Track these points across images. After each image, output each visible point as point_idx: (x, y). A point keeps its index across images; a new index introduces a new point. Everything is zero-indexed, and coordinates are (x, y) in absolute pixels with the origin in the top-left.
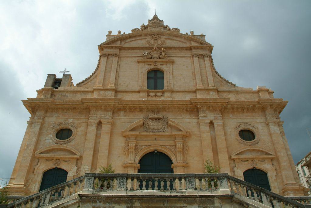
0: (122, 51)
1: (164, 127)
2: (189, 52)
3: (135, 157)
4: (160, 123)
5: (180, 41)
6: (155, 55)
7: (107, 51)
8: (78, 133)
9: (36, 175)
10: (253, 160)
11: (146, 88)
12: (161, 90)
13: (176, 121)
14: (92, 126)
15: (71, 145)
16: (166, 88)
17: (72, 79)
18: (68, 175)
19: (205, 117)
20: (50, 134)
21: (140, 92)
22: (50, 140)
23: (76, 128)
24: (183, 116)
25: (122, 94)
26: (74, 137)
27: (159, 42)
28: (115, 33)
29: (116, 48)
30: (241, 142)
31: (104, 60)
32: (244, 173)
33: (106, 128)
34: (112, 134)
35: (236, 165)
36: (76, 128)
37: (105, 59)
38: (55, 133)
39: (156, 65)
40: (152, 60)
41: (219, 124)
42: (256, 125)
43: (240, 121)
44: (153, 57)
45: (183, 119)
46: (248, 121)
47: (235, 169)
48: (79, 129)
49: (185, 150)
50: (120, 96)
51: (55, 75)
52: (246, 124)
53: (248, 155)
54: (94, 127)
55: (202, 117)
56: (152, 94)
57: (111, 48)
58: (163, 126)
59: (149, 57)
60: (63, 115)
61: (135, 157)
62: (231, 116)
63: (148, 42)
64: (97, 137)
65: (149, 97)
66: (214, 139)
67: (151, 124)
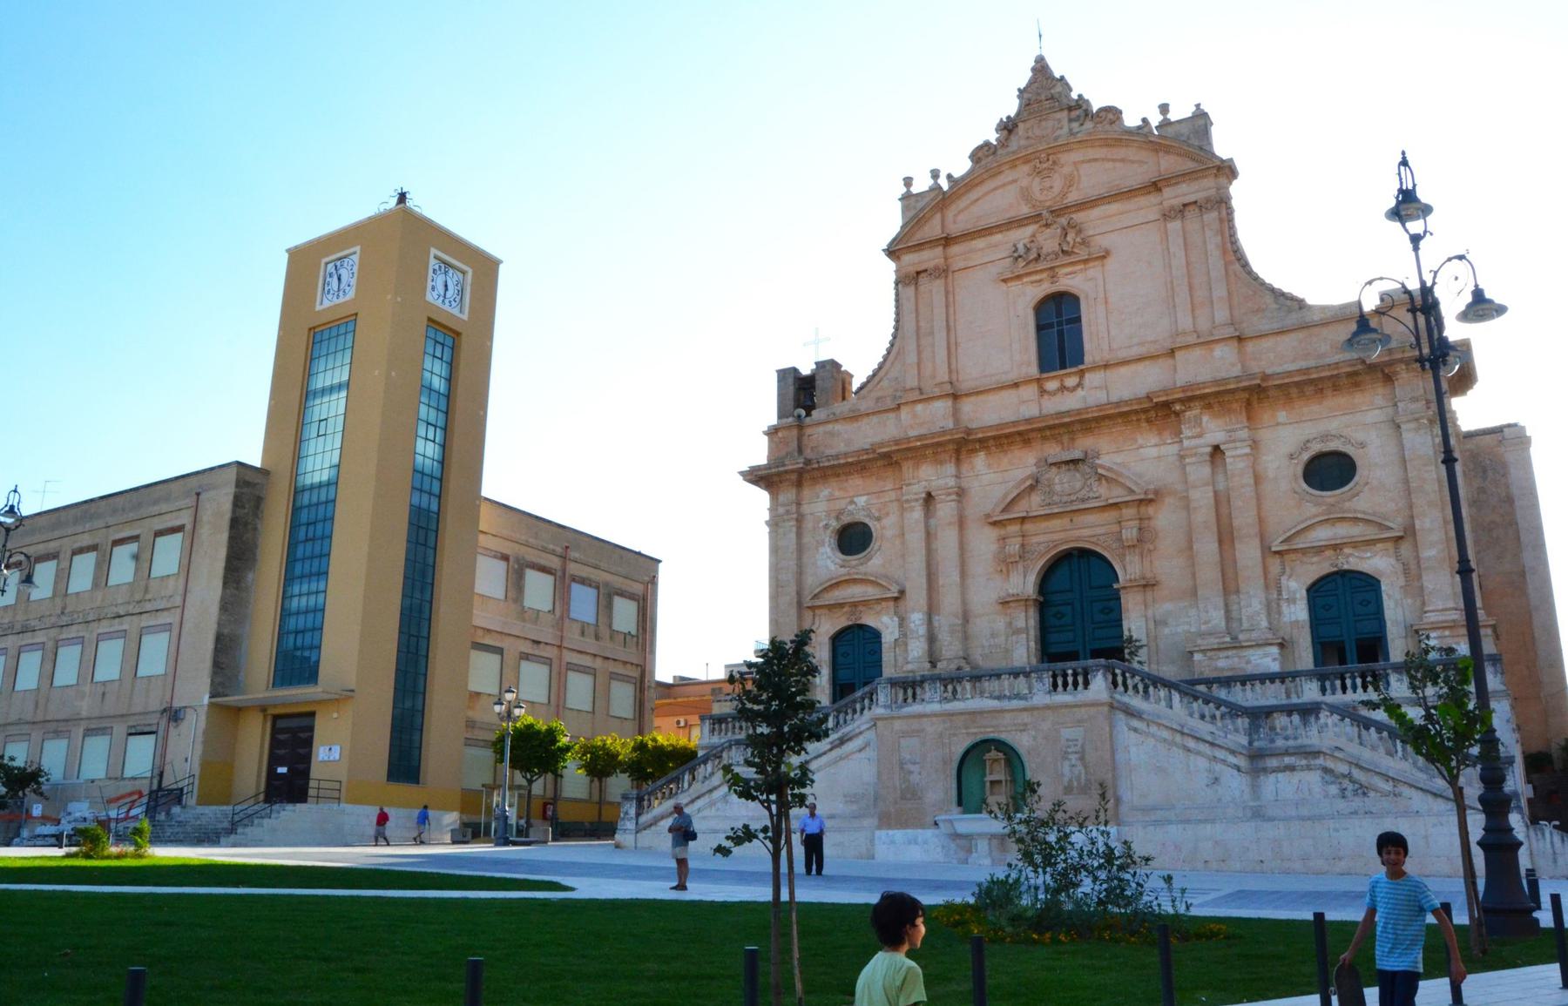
0: (955, 249)
1: (1089, 482)
2: (1153, 199)
3: (1025, 577)
4: (1078, 470)
5: (1122, 160)
6: (1049, 241)
7: (912, 260)
8: (885, 530)
9: (818, 648)
10: (1337, 547)
11: (1033, 370)
12: (1073, 370)
13: (1119, 459)
14: (912, 509)
15: (875, 561)
16: (1088, 358)
17: (840, 366)
18: (883, 640)
19: (1200, 436)
20: (824, 545)
21: (1160, 190)
22: (827, 561)
23: (878, 519)
24: (1140, 441)
25: (972, 399)
26: (878, 544)
27: (1057, 183)
28: (922, 185)
29: (932, 243)
30: (1308, 497)
31: (910, 291)
32: (1308, 590)
33: (945, 510)
34: (961, 523)
35: (1288, 569)
36: (878, 519)
37: (910, 291)
38: (834, 542)
39: (1054, 278)
40: (1040, 266)
41: (1239, 452)
42: (1359, 436)
43: (1309, 430)
44: (1044, 251)
45: (1142, 450)
46: (1333, 425)
47: (1284, 580)
48: (886, 522)
49: (1144, 540)
50: (967, 406)
51: (795, 370)
52: (1325, 437)
53: (1322, 535)
54: (917, 514)
55: (1189, 438)
56: (1052, 385)
57: (920, 246)
58: (1087, 479)
59: (1032, 257)
60: (840, 489)
61: (1025, 577)
62: (1282, 416)
63: (1026, 195)
64: (929, 536)
65: (1046, 397)
66: (1221, 502)
67: (1057, 481)
